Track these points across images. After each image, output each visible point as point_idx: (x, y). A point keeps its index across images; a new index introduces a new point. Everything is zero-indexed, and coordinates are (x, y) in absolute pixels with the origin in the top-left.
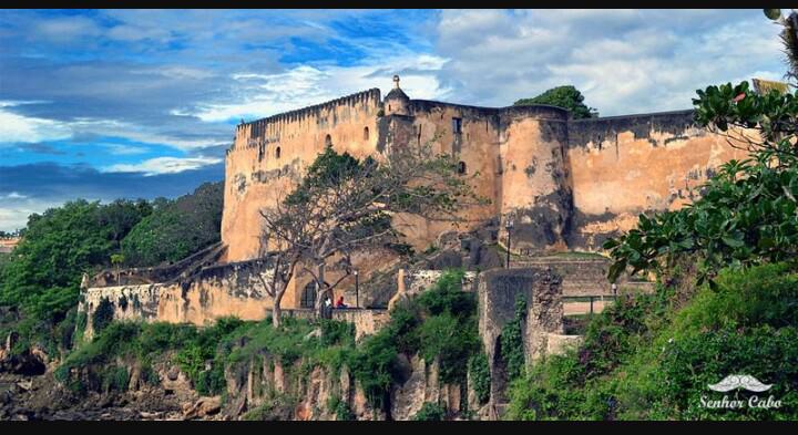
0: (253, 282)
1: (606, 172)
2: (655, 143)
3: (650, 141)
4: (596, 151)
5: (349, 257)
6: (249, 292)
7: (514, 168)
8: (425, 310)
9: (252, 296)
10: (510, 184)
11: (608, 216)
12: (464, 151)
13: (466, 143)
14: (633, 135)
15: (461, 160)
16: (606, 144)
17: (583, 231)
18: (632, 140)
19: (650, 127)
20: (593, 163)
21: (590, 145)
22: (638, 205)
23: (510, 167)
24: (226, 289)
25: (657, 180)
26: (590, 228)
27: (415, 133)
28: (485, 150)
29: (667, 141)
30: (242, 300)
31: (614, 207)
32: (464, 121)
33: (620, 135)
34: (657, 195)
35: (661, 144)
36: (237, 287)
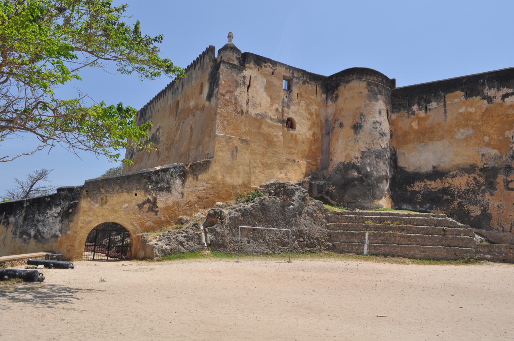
0: (38, 221)
1: (433, 132)
2: (490, 100)
3: (484, 98)
4: (422, 113)
5: (155, 199)
6: (33, 233)
7: (341, 125)
8: (157, 218)
9: (35, 237)
10: (337, 140)
11: (437, 174)
12: (293, 108)
13: (296, 101)
14: (463, 94)
15: (291, 116)
16: (433, 105)
17: (409, 189)
18: (463, 99)
19: (483, 84)
20: (419, 124)
21: (415, 108)
22: (471, 162)
23: (337, 124)
24: (11, 227)
25: (495, 137)
26: (417, 186)
27: (244, 83)
28: (313, 111)
29: (505, 97)
30: (25, 241)
31: (442, 165)
32: (295, 80)
33: (448, 95)
34: (494, 152)
35: (498, 100)
36: (22, 226)
